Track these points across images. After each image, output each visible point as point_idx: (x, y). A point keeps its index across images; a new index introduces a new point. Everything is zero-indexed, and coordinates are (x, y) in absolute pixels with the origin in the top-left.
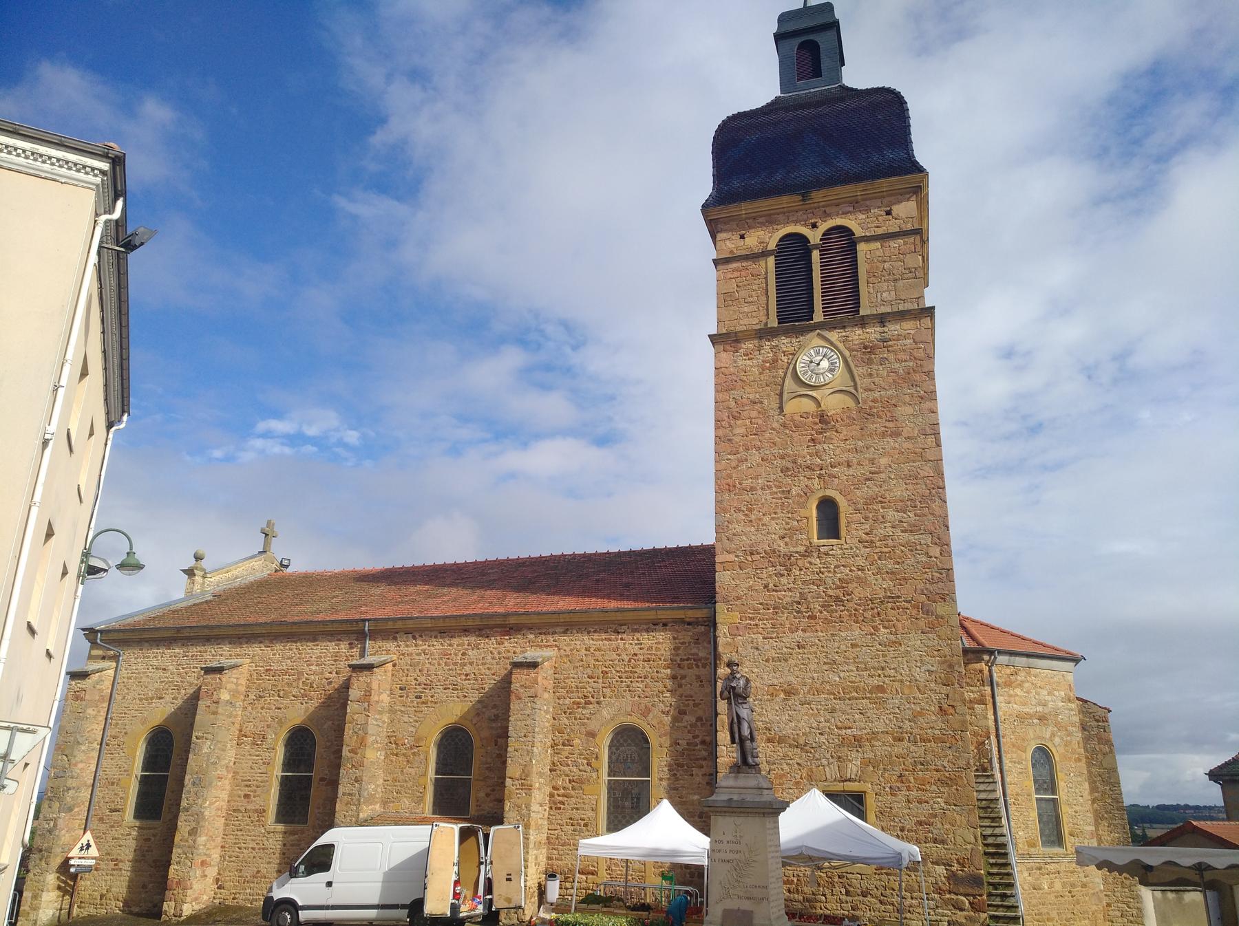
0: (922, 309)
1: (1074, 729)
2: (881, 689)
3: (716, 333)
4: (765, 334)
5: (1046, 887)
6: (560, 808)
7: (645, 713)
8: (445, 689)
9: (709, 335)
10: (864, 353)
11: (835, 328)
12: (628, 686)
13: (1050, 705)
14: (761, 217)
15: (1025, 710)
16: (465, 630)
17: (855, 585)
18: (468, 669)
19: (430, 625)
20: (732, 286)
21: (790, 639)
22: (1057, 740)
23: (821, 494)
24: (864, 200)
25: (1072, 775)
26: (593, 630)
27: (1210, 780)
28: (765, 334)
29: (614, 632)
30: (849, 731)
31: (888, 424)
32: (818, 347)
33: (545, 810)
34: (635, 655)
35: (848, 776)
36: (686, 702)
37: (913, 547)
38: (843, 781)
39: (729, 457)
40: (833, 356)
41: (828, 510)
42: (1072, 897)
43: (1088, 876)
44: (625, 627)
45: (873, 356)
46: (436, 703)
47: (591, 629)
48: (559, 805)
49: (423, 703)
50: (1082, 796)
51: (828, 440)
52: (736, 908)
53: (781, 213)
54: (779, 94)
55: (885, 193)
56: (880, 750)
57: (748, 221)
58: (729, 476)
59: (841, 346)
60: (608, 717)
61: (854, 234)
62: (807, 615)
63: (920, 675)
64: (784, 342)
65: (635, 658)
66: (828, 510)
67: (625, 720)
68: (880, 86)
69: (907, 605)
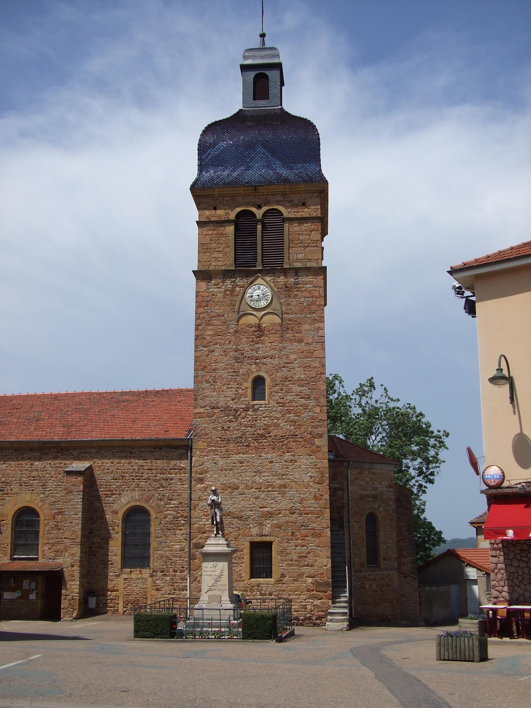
0: (319, 267)
1: (391, 503)
2: (284, 486)
3: (197, 270)
4: (227, 274)
5: (368, 587)
6: (95, 555)
7: (147, 501)
8: (20, 485)
9: (193, 271)
10: (285, 291)
11: (269, 273)
12: (138, 485)
13: (380, 490)
14: (227, 197)
15: (365, 493)
16: (32, 450)
17: (273, 428)
18: (34, 473)
19: (8, 446)
20: (208, 240)
21: (236, 458)
22: (381, 509)
23: (256, 374)
24: (290, 194)
25: (388, 527)
26: (115, 451)
27: (441, 532)
28: (227, 274)
29: (129, 452)
30: (266, 509)
31: (296, 335)
32: (258, 284)
33: (87, 556)
34: (142, 466)
35: (264, 533)
36: (173, 494)
37: (306, 407)
38: (261, 536)
39: (203, 348)
40: (267, 290)
41: (259, 382)
42: (382, 591)
43: (391, 581)
44: (136, 450)
45: (291, 293)
46: (14, 494)
47: (114, 451)
48: (95, 553)
49: (5, 494)
50: (392, 539)
51: (263, 342)
52: (214, 594)
53: (240, 196)
54: (241, 108)
55: (302, 192)
56: (281, 519)
57: (219, 198)
58: (204, 361)
59: (272, 284)
60: (125, 502)
61: (282, 215)
62: (245, 444)
63: (307, 479)
64: (240, 282)
65: (142, 468)
66: (259, 382)
67: (135, 504)
68: (305, 117)
69: (301, 440)
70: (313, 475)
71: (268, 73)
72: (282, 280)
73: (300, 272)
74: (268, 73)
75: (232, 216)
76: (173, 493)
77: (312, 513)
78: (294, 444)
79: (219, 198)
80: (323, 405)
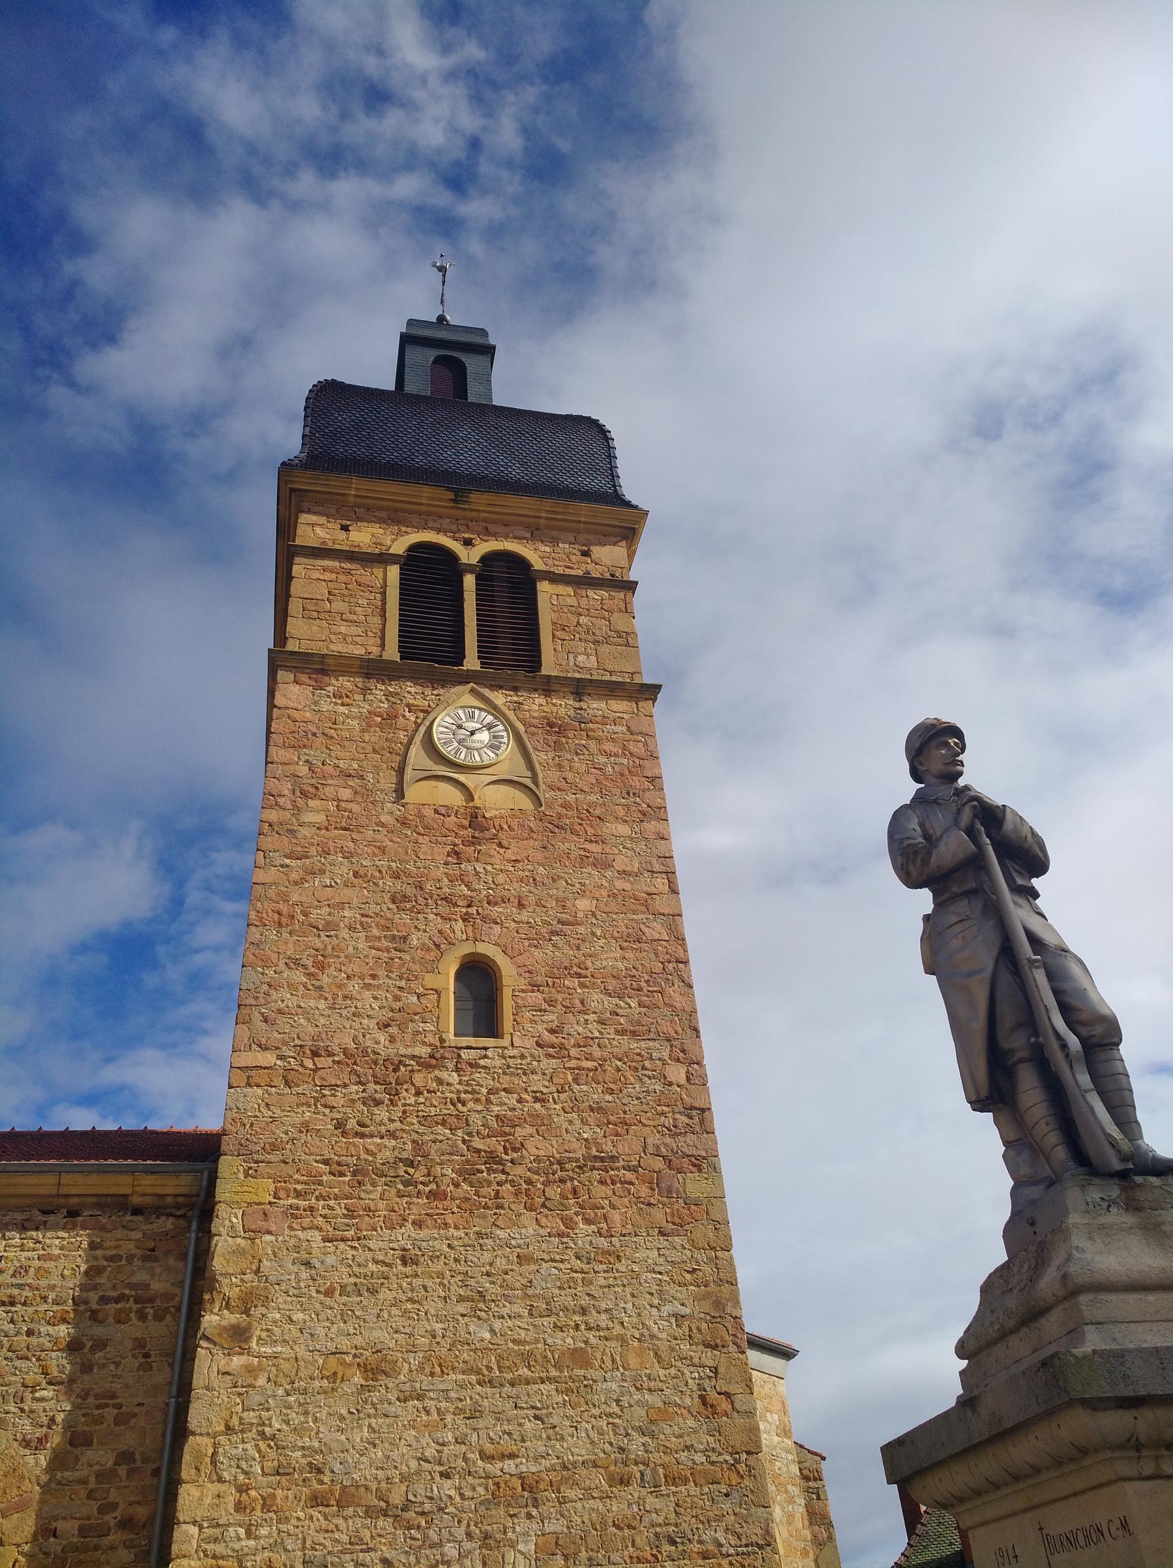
17: (530, 1130)
23: (467, 949)
30: (510, 1465)
37: (637, 1063)
57: (357, 510)
70: (687, 1311)
71: (464, 357)
72: (536, 704)
73: (589, 695)
74: (464, 357)
75: (399, 547)
76: (98, 1407)
77: (695, 1476)
78: (606, 1190)
79: (357, 510)
80: (644, 730)
